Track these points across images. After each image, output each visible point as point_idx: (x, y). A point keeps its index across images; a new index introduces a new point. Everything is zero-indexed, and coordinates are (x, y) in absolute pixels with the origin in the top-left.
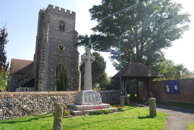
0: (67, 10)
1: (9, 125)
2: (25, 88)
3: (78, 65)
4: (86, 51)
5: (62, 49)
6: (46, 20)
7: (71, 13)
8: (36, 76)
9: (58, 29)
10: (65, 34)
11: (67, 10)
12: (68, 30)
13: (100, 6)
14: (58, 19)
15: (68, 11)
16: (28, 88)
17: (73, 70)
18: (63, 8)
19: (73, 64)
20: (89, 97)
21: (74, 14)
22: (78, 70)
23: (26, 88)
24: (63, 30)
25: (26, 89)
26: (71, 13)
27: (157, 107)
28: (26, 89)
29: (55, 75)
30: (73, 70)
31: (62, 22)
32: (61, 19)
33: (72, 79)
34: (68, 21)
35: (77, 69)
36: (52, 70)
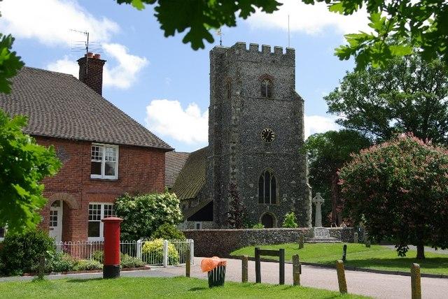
0: (276, 49)
1: (99, 281)
2: (196, 223)
3: (304, 171)
4: (394, 117)
5: (269, 139)
6: (232, 74)
7: (284, 52)
8: (215, 198)
9: (260, 94)
10: (274, 105)
11: (276, 49)
12: (279, 92)
13: (199, 107)
14: (258, 71)
15: (278, 49)
16: (201, 223)
17: (294, 182)
18: (267, 44)
19: (294, 169)
20: (76, 246)
21: (291, 53)
22: (304, 184)
23: (198, 223)
24: (270, 95)
25: (198, 225)
26: (284, 52)
27: (196, 255)
28: (198, 225)
29: (257, 196)
30: (294, 182)
31: (267, 77)
32: (264, 70)
33: (294, 202)
34: (278, 74)
35: (303, 181)
36: (252, 185)
